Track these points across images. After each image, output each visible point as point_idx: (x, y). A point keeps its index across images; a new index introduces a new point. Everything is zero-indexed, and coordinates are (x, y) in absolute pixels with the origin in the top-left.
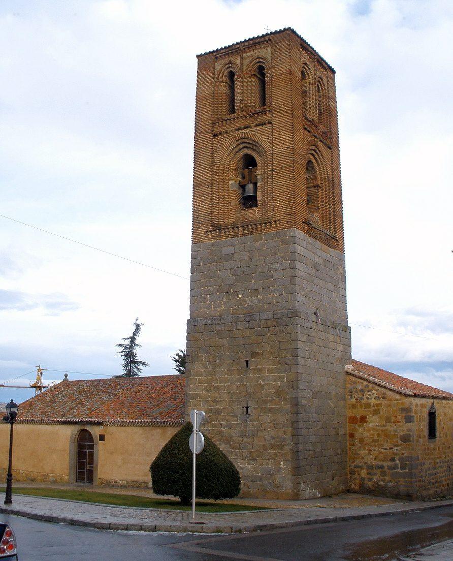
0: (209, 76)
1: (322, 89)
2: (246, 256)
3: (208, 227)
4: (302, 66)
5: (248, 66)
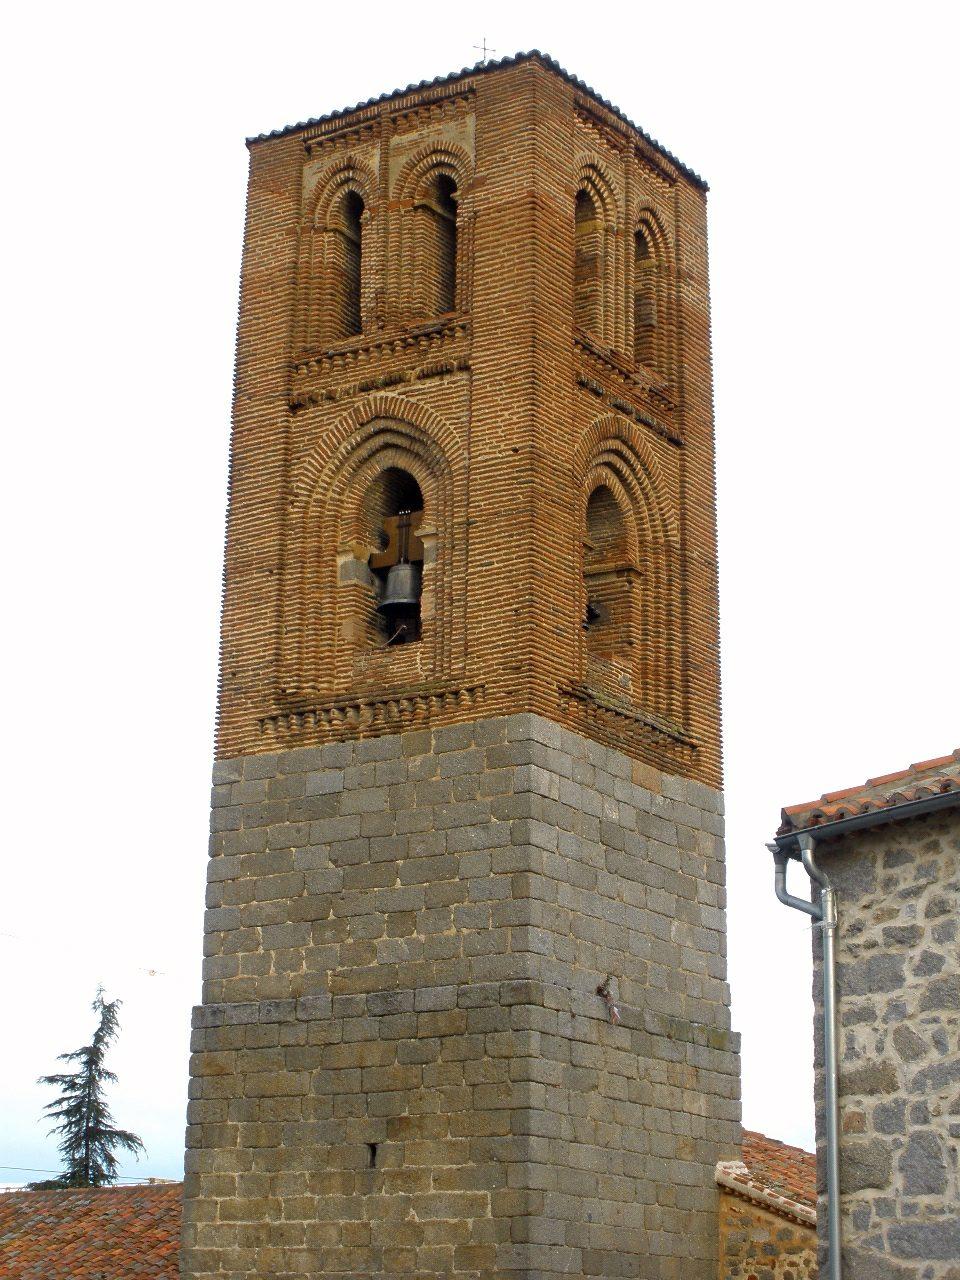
0: (284, 208)
1: (656, 245)
2: (378, 800)
3: (269, 704)
4: (584, 173)
5: (404, 177)
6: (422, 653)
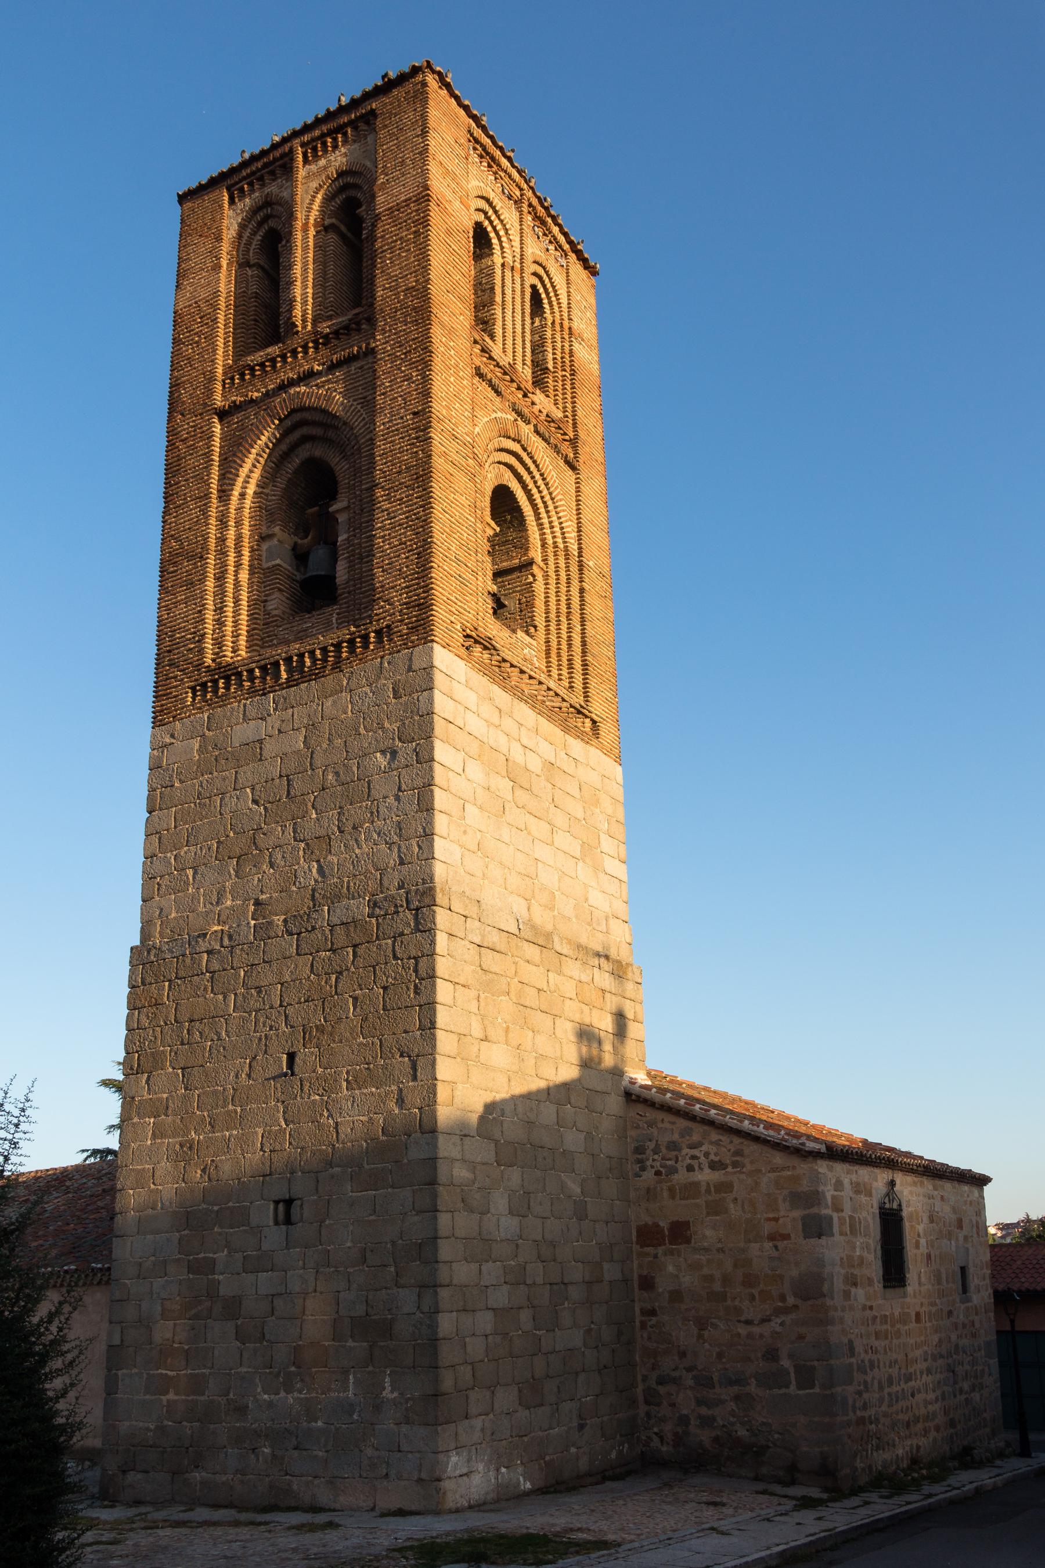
6: (338, 614)
